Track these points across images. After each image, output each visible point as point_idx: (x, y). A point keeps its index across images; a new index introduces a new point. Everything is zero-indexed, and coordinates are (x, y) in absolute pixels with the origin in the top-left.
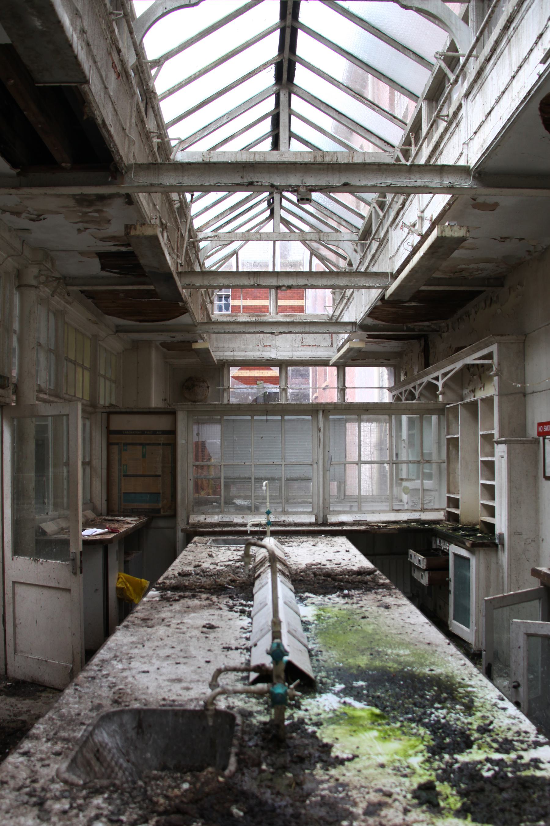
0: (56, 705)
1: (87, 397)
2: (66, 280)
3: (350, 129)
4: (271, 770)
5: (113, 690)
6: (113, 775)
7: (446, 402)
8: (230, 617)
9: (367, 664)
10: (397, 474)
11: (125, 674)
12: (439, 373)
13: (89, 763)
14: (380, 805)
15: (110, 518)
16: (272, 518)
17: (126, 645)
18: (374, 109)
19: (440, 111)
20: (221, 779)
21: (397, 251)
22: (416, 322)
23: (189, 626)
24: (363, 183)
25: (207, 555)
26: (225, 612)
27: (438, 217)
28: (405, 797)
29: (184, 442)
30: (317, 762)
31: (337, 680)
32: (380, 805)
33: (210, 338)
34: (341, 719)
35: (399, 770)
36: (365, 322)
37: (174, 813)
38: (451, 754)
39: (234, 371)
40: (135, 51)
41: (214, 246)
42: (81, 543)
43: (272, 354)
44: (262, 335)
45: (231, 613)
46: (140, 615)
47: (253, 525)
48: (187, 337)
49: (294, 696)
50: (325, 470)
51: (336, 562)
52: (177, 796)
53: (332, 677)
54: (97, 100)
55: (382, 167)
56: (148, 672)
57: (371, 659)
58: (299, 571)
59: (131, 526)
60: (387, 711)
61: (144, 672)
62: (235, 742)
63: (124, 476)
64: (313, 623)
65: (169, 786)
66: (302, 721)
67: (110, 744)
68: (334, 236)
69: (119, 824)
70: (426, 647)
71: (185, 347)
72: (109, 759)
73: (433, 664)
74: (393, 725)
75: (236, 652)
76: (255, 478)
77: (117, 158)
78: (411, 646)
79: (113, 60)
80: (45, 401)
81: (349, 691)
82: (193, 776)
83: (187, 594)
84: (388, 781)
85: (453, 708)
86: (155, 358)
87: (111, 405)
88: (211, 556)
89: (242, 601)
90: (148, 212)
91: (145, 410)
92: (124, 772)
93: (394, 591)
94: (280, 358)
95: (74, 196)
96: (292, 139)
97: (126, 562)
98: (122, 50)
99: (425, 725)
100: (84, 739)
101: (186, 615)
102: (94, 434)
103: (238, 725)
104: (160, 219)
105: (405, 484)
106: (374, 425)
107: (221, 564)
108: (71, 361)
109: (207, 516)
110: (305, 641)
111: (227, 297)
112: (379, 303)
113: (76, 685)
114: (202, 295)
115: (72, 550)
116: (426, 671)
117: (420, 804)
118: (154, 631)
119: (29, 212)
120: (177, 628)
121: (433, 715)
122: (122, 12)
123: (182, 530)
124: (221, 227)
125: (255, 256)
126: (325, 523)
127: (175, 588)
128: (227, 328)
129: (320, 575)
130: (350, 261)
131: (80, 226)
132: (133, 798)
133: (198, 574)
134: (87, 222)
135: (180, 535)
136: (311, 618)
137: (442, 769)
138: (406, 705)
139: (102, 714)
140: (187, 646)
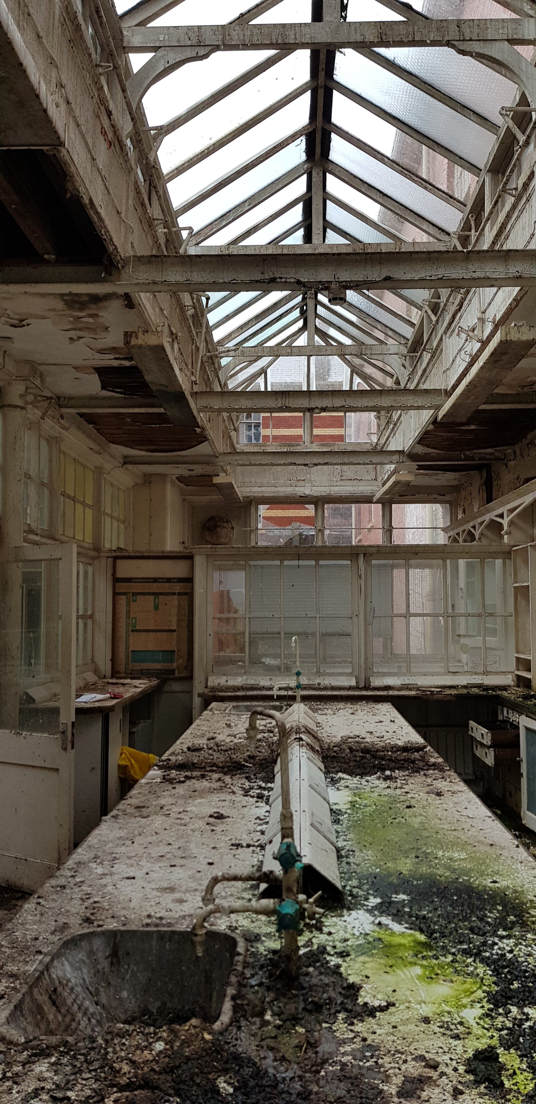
0: (9, 926)
1: (89, 539)
2: (60, 401)
3: (397, 214)
4: (278, 1022)
5: (86, 904)
6: (74, 1025)
7: (512, 543)
8: (244, 803)
9: (411, 870)
10: (454, 630)
11: (103, 881)
12: (504, 509)
13: (40, 1010)
14: (422, 1081)
15: (114, 681)
16: (304, 680)
17: (112, 841)
18: (425, 188)
19: (506, 183)
20: (207, 1037)
21: (452, 363)
22: (476, 449)
23: (193, 815)
24: (409, 276)
25: (224, 725)
26: (239, 798)
27: (502, 317)
28: (455, 1070)
29: (202, 591)
30: (339, 1012)
31: (371, 892)
32: (422, 1081)
33: (234, 471)
34: (375, 948)
35: (448, 1028)
36: (415, 451)
37: (141, 1087)
38: (521, 1007)
39: (263, 510)
40: (130, 114)
41: (237, 363)
42: (73, 712)
43: (307, 490)
44: (295, 467)
45: (246, 798)
46: (134, 801)
47: (280, 689)
48: (208, 470)
49: (314, 913)
50: (367, 623)
51: (377, 735)
52: (145, 1062)
53: (365, 887)
54: (81, 174)
55: (432, 255)
56: (134, 878)
57: (417, 863)
58: (332, 745)
59: (139, 690)
60: (435, 938)
61: (128, 878)
62: (233, 979)
63: (132, 631)
64: (346, 813)
65: (138, 1047)
66: (322, 950)
67: (73, 980)
68: (379, 349)
69: (66, 1102)
70: (488, 849)
71: (204, 481)
72: (69, 1002)
73: (497, 873)
74: (443, 958)
75: (247, 850)
76: (285, 633)
77: (111, 249)
78: (469, 847)
79: (102, 124)
80: (35, 543)
81: (387, 907)
82: (171, 1031)
83: (196, 773)
84: (432, 1044)
85: (523, 937)
86: (171, 495)
87: (119, 549)
88: (229, 726)
89: (261, 783)
90: (153, 318)
91: (157, 554)
92: (89, 1020)
93: (448, 773)
94: (315, 494)
95: (62, 295)
96: (329, 231)
97: (131, 734)
98: (114, 112)
99: (485, 961)
100: (37, 974)
101: (190, 801)
102: (97, 582)
103: (239, 954)
104: (169, 327)
105: (463, 641)
106: (427, 571)
107: (240, 735)
108: (69, 497)
109: (229, 677)
110: (333, 838)
111: (257, 426)
112: (431, 427)
113: (39, 897)
114: (224, 421)
115: (62, 719)
116: (488, 882)
117: (477, 1083)
118: (148, 823)
119: (9, 317)
120: (178, 819)
121: (496, 947)
122: (111, 65)
123: (199, 695)
124: (246, 340)
125: (287, 373)
126: (367, 687)
127: (181, 767)
128: (253, 459)
129: (357, 751)
130: (397, 378)
131: (73, 334)
132: (90, 1063)
133: (211, 749)
134: (80, 329)
135: (197, 701)
136: (343, 807)
137: (508, 1029)
138: (460, 931)
139: (65, 939)
140: (187, 842)
